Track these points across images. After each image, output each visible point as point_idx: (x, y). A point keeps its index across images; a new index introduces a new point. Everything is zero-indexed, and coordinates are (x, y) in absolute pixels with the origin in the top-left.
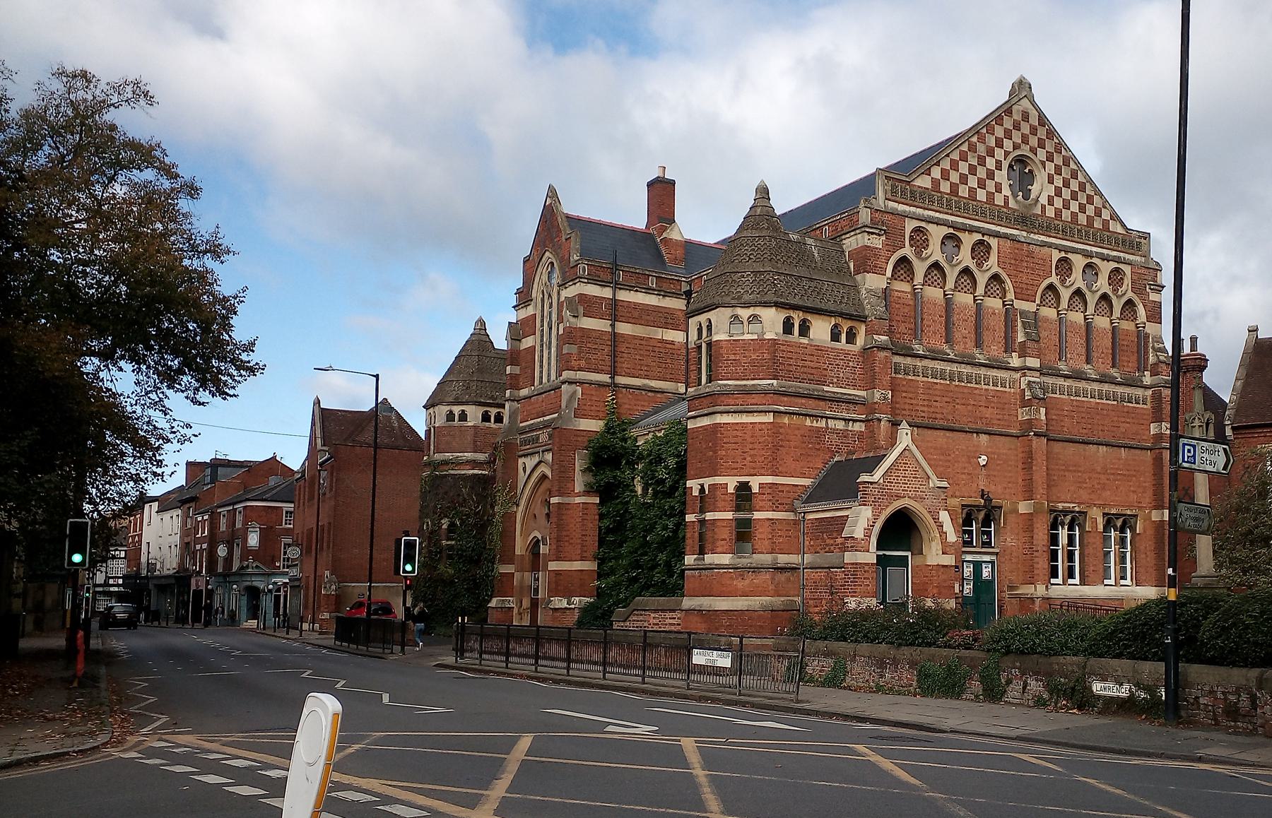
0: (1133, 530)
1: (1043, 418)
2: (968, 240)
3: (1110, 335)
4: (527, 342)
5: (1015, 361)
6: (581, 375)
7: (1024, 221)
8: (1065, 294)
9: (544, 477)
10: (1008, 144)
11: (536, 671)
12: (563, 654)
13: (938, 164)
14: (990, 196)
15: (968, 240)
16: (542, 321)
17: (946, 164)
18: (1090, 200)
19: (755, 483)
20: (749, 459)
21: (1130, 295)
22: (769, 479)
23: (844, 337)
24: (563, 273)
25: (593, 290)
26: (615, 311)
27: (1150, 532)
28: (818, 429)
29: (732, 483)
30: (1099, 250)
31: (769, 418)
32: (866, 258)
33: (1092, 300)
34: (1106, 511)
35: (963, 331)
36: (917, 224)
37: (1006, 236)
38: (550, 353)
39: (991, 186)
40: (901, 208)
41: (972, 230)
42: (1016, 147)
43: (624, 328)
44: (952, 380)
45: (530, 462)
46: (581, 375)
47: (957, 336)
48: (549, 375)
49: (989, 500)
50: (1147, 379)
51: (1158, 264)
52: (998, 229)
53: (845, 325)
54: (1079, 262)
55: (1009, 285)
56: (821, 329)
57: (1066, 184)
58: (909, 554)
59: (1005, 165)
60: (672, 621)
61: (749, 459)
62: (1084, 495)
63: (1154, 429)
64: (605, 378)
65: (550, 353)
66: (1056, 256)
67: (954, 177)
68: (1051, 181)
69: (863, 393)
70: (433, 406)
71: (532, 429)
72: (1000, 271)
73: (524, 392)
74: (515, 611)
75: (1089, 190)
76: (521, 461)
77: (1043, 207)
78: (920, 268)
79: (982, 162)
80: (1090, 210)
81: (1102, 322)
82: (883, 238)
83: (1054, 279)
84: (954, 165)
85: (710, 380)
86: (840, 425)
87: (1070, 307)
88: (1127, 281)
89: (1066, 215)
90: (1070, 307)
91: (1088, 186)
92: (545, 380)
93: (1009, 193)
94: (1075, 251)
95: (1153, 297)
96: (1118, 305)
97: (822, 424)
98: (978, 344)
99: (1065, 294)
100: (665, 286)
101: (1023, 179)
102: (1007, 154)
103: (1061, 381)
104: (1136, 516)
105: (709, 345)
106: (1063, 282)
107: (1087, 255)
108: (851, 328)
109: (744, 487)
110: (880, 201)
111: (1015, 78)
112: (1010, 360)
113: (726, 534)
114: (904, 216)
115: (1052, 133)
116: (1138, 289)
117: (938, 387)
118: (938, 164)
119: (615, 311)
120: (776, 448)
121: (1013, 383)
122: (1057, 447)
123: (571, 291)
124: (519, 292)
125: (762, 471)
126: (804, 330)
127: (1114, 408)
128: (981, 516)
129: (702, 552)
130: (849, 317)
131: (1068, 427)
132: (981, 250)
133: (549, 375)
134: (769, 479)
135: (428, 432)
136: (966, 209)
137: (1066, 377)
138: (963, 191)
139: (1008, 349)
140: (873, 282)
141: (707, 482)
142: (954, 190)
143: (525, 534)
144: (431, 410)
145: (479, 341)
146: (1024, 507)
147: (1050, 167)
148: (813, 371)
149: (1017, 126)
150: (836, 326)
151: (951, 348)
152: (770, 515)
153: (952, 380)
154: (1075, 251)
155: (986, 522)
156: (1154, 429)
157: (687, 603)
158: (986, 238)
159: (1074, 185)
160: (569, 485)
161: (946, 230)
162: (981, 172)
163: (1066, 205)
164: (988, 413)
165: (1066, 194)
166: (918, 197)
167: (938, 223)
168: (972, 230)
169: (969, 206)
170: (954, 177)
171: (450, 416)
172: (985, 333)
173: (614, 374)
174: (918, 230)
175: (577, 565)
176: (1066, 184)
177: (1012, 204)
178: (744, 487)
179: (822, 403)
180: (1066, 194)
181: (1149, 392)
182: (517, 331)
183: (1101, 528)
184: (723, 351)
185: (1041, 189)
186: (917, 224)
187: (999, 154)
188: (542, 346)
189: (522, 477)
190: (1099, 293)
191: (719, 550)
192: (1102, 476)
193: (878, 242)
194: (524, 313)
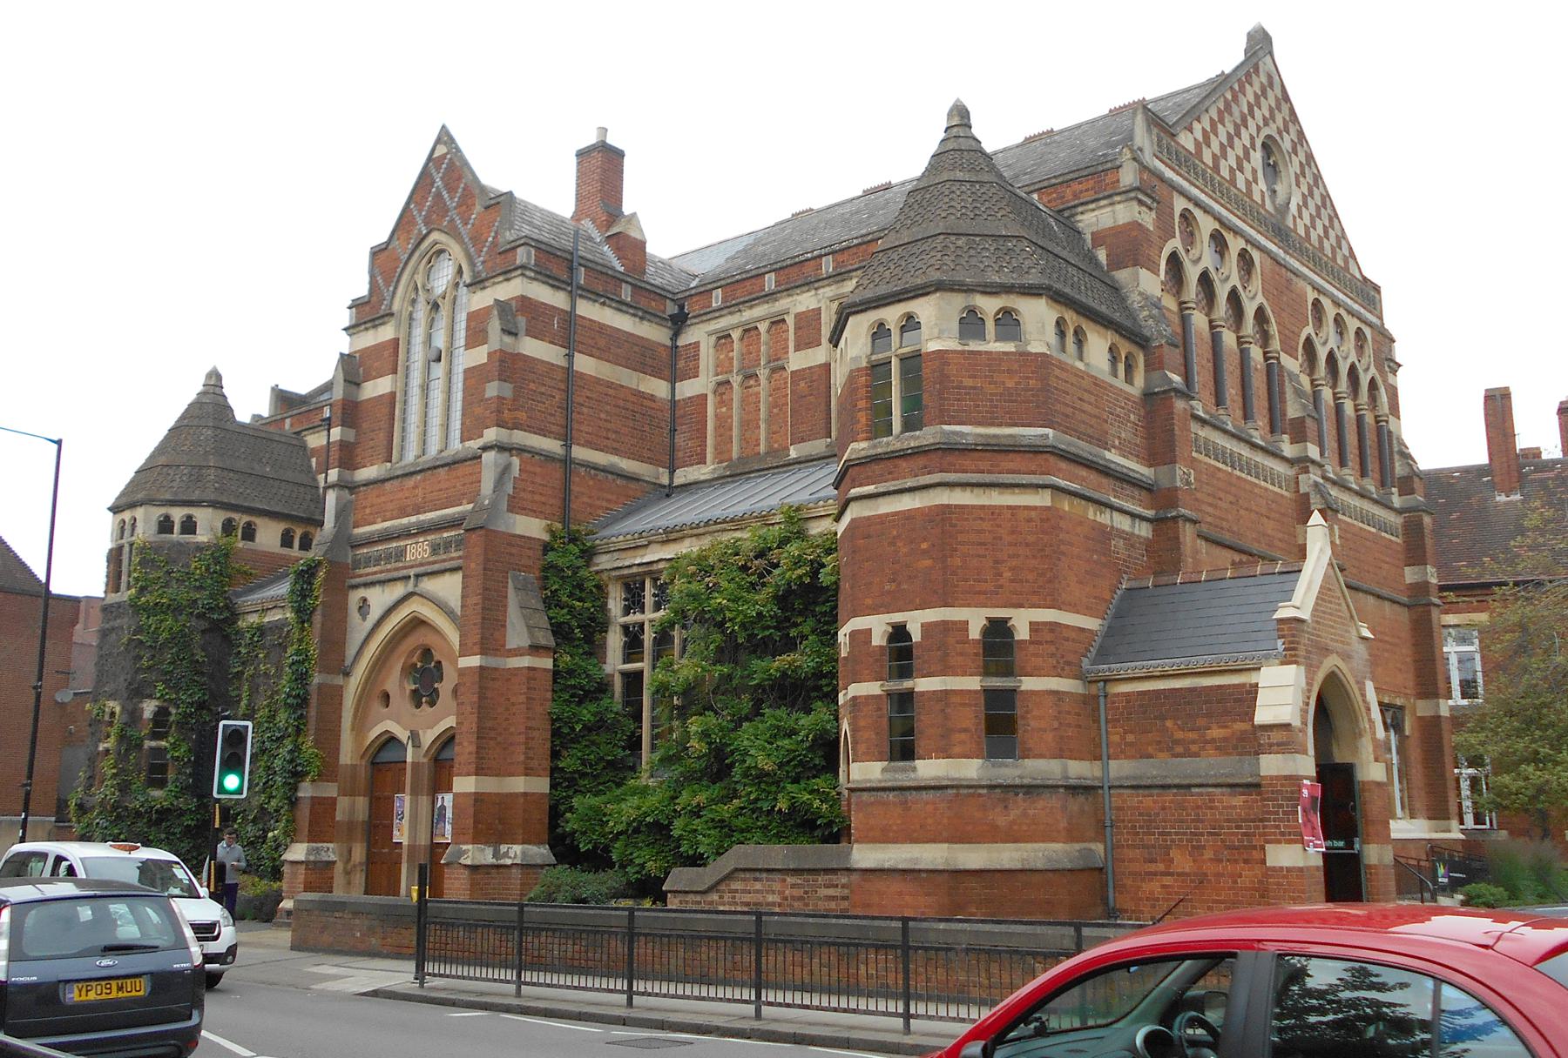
4: (377, 388)
5: (1288, 449)
11: (518, 994)
12: (894, 979)
17: (1214, 114)
19: (1022, 621)
20: (1007, 575)
25: (543, 294)
26: (570, 332)
29: (975, 620)
31: (1042, 499)
43: (585, 364)
45: (379, 599)
60: (831, 892)
61: (1007, 575)
63: (1410, 575)
64: (552, 445)
70: (132, 506)
71: (387, 537)
74: (339, 867)
85: (910, 425)
97: (1105, 518)
100: (643, 303)
109: (998, 630)
111: (208, 369)
113: (971, 719)
117: (1221, 475)
119: (570, 332)
124: (357, 305)
125: (1035, 599)
126: (249, 533)
143: (360, 725)
144: (127, 515)
157: (864, 856)
160: (497, 634)
171: (165, 526)
173: (568, 440)
175: (518, 784)
178: (998, 630)
179: (1104, 481)
189: (358, 628)
191: (957, 750)
194: (369, 339)
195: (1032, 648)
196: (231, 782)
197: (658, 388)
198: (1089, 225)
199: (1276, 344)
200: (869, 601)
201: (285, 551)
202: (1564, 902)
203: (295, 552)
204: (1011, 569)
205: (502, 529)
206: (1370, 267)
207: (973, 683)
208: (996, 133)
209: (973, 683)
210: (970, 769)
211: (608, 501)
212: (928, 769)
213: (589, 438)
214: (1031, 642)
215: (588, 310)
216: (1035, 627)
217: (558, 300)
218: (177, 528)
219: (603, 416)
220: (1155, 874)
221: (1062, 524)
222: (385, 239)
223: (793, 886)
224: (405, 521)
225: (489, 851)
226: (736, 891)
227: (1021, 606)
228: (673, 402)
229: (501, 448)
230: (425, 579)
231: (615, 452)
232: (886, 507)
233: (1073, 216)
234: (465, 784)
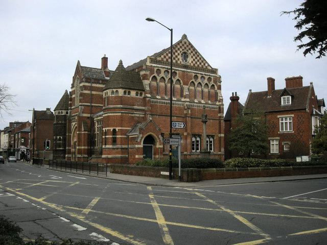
4: (73, 96)
7: (186, 67)
10: (181, 50)
14: (176, 61)
18: (202, 61)
19: (117, 129)
27: (218, 139)
29: (112, 129)
31: (120, 114)
39: (176, 59)
40: (153, 65)
42: (183, 50)
43: (94, 93)
54: (200, 76)
56: (133, 93)
57: (196, 58)
59: (180, 54)
66: (194, 75)
73: (73, 107)
80: (202, 64)
81: (206, 90)
83: (193, 80)
93: (181, 61)
97: (133, 115)
102: (181, 52)
107: (201, 74)
109: (114, 130)
116: (215, 82)
119: (91, 89)
120: (122, 120)
123: (82, 85)
152: (120, 136)
154: (198, 73)
159: (198, 58)
163: (196, 63)
171: (59, 113)
175: (83, 147)
176: (196, 58)
178: (114, 130)
180: (196, 60)
181: (218, 106)
187: (179, 52)
199: (182, 84)
201: (137, 97)
202: (325, 173)
203: (139, 96)
206: (214, 65)
207: (111, 136)
208: (125, 65)
209: (111, 136)
210: (111, 146)
215: (94, 85)
232: (110, 114)
234: (77, 147)
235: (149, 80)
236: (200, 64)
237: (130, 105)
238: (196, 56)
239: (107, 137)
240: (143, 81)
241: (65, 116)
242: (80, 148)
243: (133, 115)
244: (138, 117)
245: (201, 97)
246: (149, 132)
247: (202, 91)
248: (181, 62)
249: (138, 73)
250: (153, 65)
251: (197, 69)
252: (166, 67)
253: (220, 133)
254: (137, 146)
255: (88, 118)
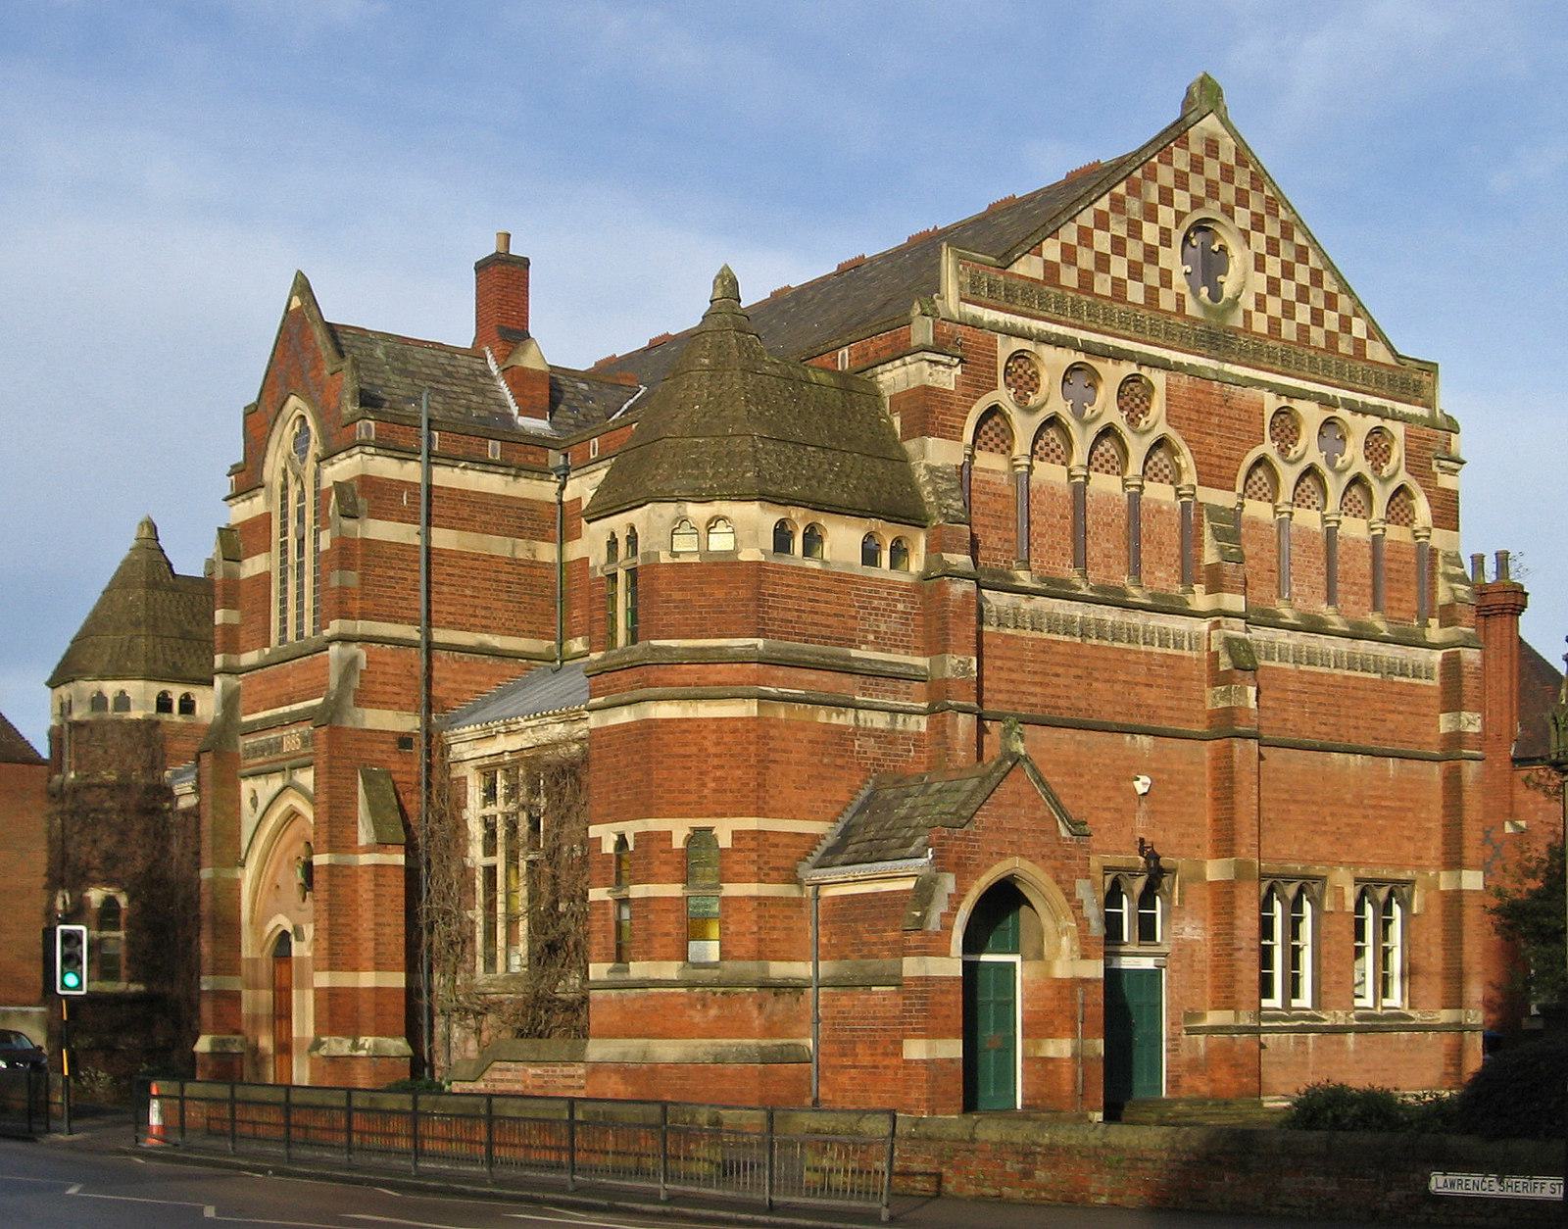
0: (1406, 906)
1: (1252, 704)
2: (1112, 374)
3: (1368, 552)
4: (253, 566)
5: (1200, 600)
6: (362, 627)
7: (1216, 339)
8: (1288, 475)
9: (294, 814)
10: (1182, 200)
13: (1054, 234)
14: (1151, 293)
15: (1112, 374)
16: (284, 525)
18: (1331, 301)
19: (725, 830)
21: (1403, 477)
22: (751, 823)
23: (885, 557)
24: (325, 437)
25: (386, 468)
27: (1436, 912)
28: (840, 732)
29: (679, 829)
30: (1348, 395)
31: (746, 709)
32: (927, 411)
33: (1335, 487)
34: (1362, 872)
35: (1104, 545)
36: (1017, 344)
37: (1178, 367)
38: (300, 586)
39: (1152, 276)
40: (988, 315)
41: (1119, 356)
42: (1197, 203)
43: (444, 538)
44: (1084, 635)
46: (362, 627)
47: (1094, 553)
48: (300, 626)
49: (1153, 857)
50: (1435, 632)
51: (1449, 418)
52: (1165, 353)
53: (887, 533)
54: (1311, 414)
55: (1186, 460)
56: (843, 540)
57: (1288, 272)
58: (1016, 958)
59: (1177, 237)
62: (1323, 846)
63: (1445, 724)
65: (300, 586)
66: (1271, 403)
67: (1085, 259)
68: (1260, 266)
69: (922, 661)
71: (267, 725)
72: (1172, 433)
73: (249, 658)
75: (1329, 284)
76: (246, 786)
77: (1247, 314)
78: (1023, 428)
79: (1135, 230)
80: (1331, 320)
81: (1354, 529)
82: (958, 371)
83: (1269, 448)
84: (1085, 236)
85: (634, 637)
86: (880, 721)
87: (1298, 500)
88: (1398, 452)
89: (1288, 330)
90: (1298, 500)
91: (1327, 276)
92: (291, 635)
93: (1186, 291)
94: (1304, 395)
95: (1445, 481)
96: (1381, 496)
97: (846, 719)
98: (1135, 571)
99: (1288, 475)
101: (1210, 267)
102: (1180, 216)
103: (1282, 637)
104: (1410, 882)
105: (633, 573)
106: (1283, 452)
107: (1325, 402)
108: (898, 540)
109: (701, 838)
110: (951, 300)
112: (1190, 598)
114: (994, 327)
115: (1259, 179)
116: (1419, 464)
117: (1061, 649)
118: (1054, 234)
119: (432, 506)
120: (764, 764)
121: (1195, 641)
122: (1274, 755)
123: (344, 468)
124: (236, 470)
126: (813, 540)
127: (1376, 688)
128: (1139, 884)
129: (620, 956)
130: (892, 516)
131: (1298, 721)
132: (1134, 396)
133: (300, 626)
134: (751, 823)
135: (55, 737)
136: (1108, 318)
137: (1294, 628)
138: (1102, 285)
139: (1187, 579)
140: (937, 453)
141: (632, 828)
142: (1086, 281)
145: (149, 561)
146: (1215, 870)
147: (1259, 241)
148: (831, 621)
149: (1197, 166)
150: (870, 536)
151: (1084, 575)
152: (753, 889)
153: (1084, 635)
154: (1304, 395)
155: (1146, 899)
156: (1445, 724)
158: (1145, 371)
159: (1302, 275)
161: (1069, 357)
162: (1134, 250)
163: (1288, 310)
164: (1150, 696)
165: (1288, 289)
166: (1013, 296)
167: (1061, 342)
168: (1119, 356)
169: (1110, 311)
170: (1085, 259)
172: (1145, 547)
174: (1017, 356)
175: (367, 979)
176: (1288, 272)
177: (1191, 308)
178: (701, 838)
180: (1288, 289)
181: (1438, 656)
182: (234, 542)
183: (1350, 904)
184: (661, 585)
185: (1240, 278)
186: (1017, 344)
187: (1166, 216)
188: (283, 572)
189: (248, 818)
190: (1350, 474)
192: (1354, 811)
193: (947, 377)
195: (736, 857)
196: (71, 980)
197: (547, 552)
198: (888, 388)
200: (600, 810)
204: (715, 780)
205: (349, 724)
211: (480, 683)
212: (638, 969)
213: (451, 618)
214: (734, 850)
216: (737, 836)
217: (412, 472)
218: (110, 705)
219: (468, 592)
220: (846, 1067)
221: (773, 732)
222: (254, 399)
223: (535, 1076)
224: (281, 710)
225: (348, 1043)
226: (495, 1080)
227: (724, 815)
228: (562, 565)
229: (345, 639)
230: (298, 771)
231: (486, 629)
233: (875, 376)
235: (955, 434)
236: (1317, 317)
237: (826, 639)
238: (1287, 253)
239: (637, 891)
240: (911, 446)
241: (151, 725)
242: (345, 980)
243: (846, 719)
244: (877, 735)
245: (1322, 591)
246: (1002, 855)
247: (1331, 534)
248: (1180, 300)
249: (856, 386)
250: (988, 315)
251: (1291, 357)
252: (1082, 335)
253: (1454, 861)
254: (911, 967)
255: (404, 741)
